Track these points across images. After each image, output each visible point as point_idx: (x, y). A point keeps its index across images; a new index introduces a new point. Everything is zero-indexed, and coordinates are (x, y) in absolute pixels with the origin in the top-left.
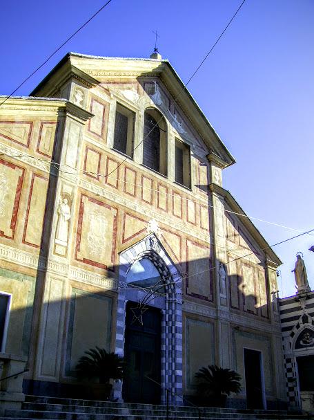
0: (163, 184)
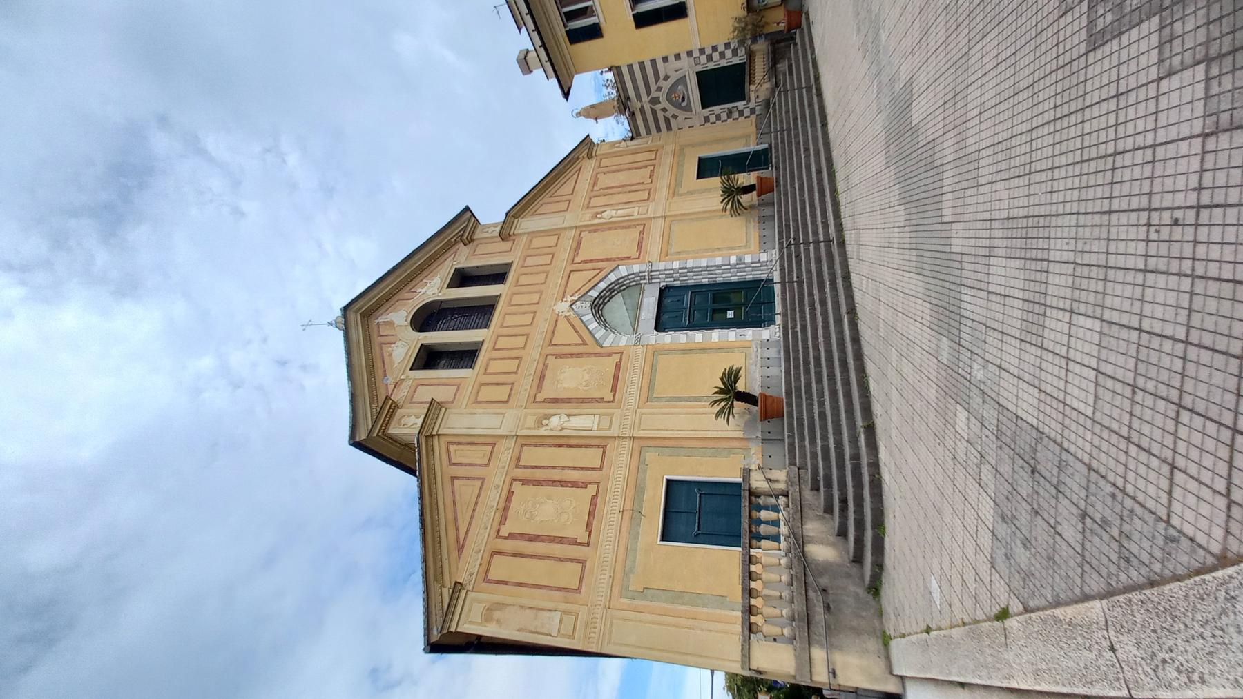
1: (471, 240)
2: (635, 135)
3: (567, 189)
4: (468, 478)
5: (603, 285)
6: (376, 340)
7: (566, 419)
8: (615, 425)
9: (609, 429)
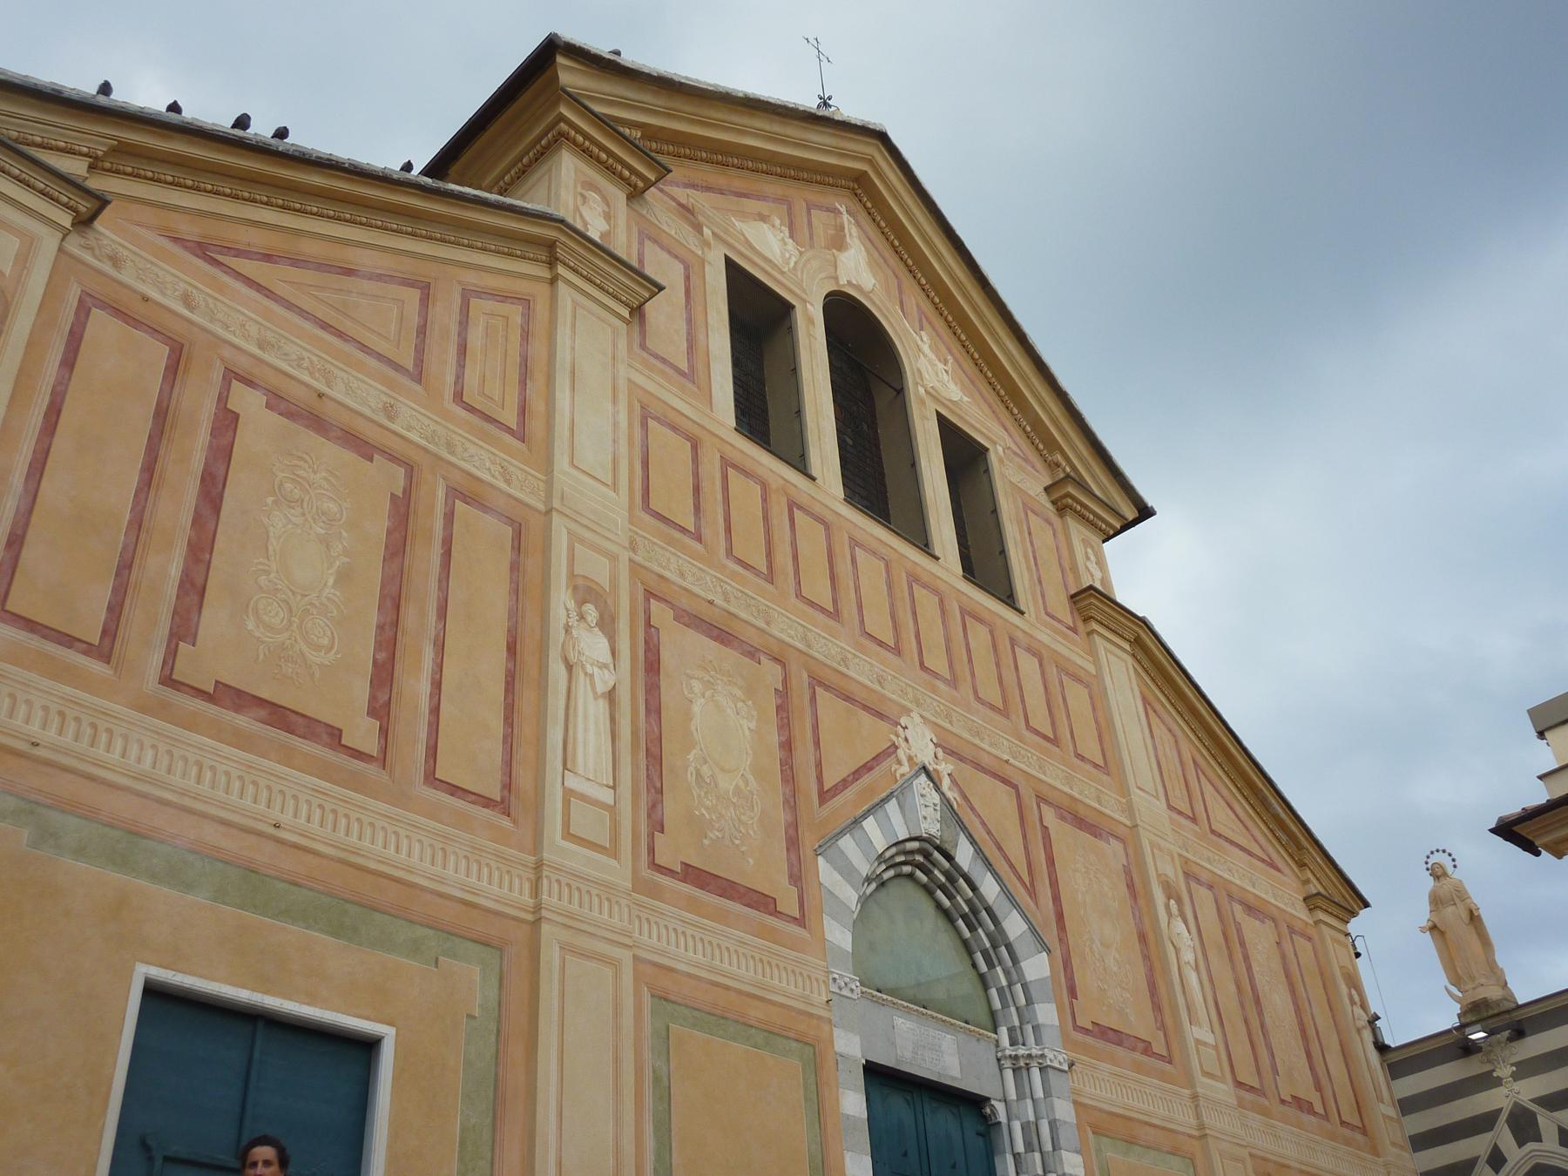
0: (925, 578)
1: (1061, 509)
2: (1394, 1058)
3: (1223, 818)
4: (422, 331)
6: (801, 195)
7: (600, 688)
8: (576, 858)
9: (568, 835)
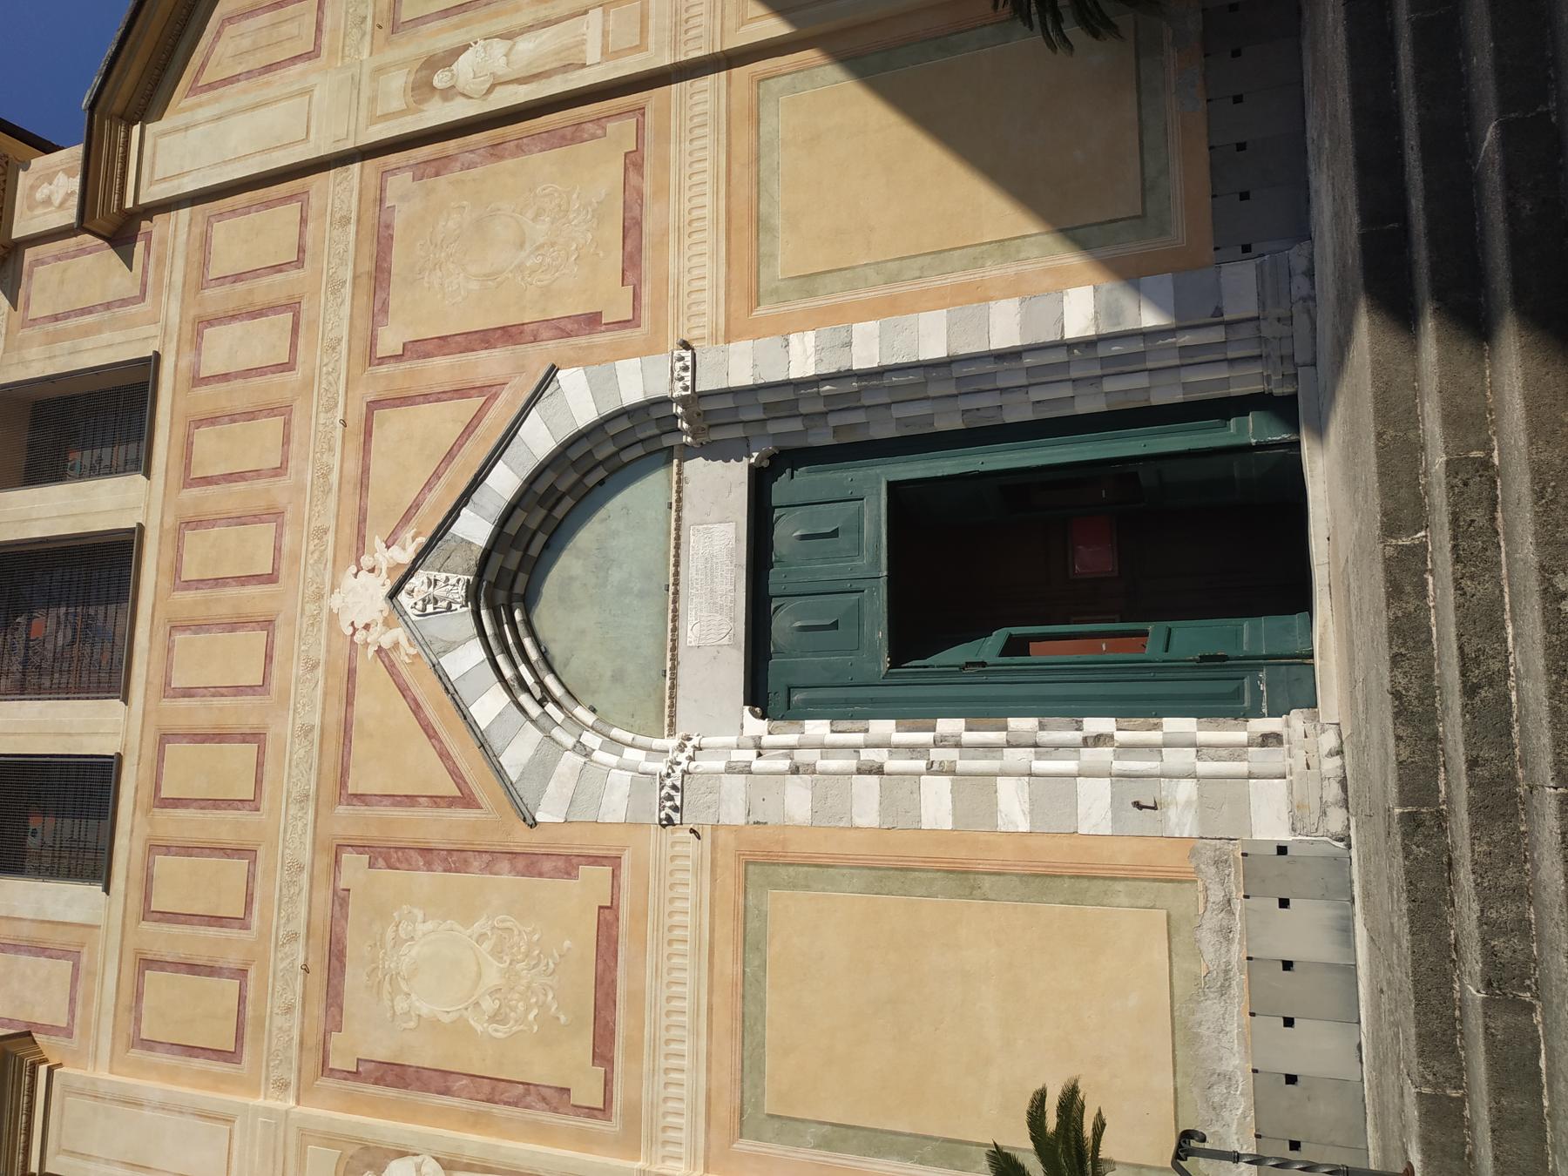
5: (505, 482)
